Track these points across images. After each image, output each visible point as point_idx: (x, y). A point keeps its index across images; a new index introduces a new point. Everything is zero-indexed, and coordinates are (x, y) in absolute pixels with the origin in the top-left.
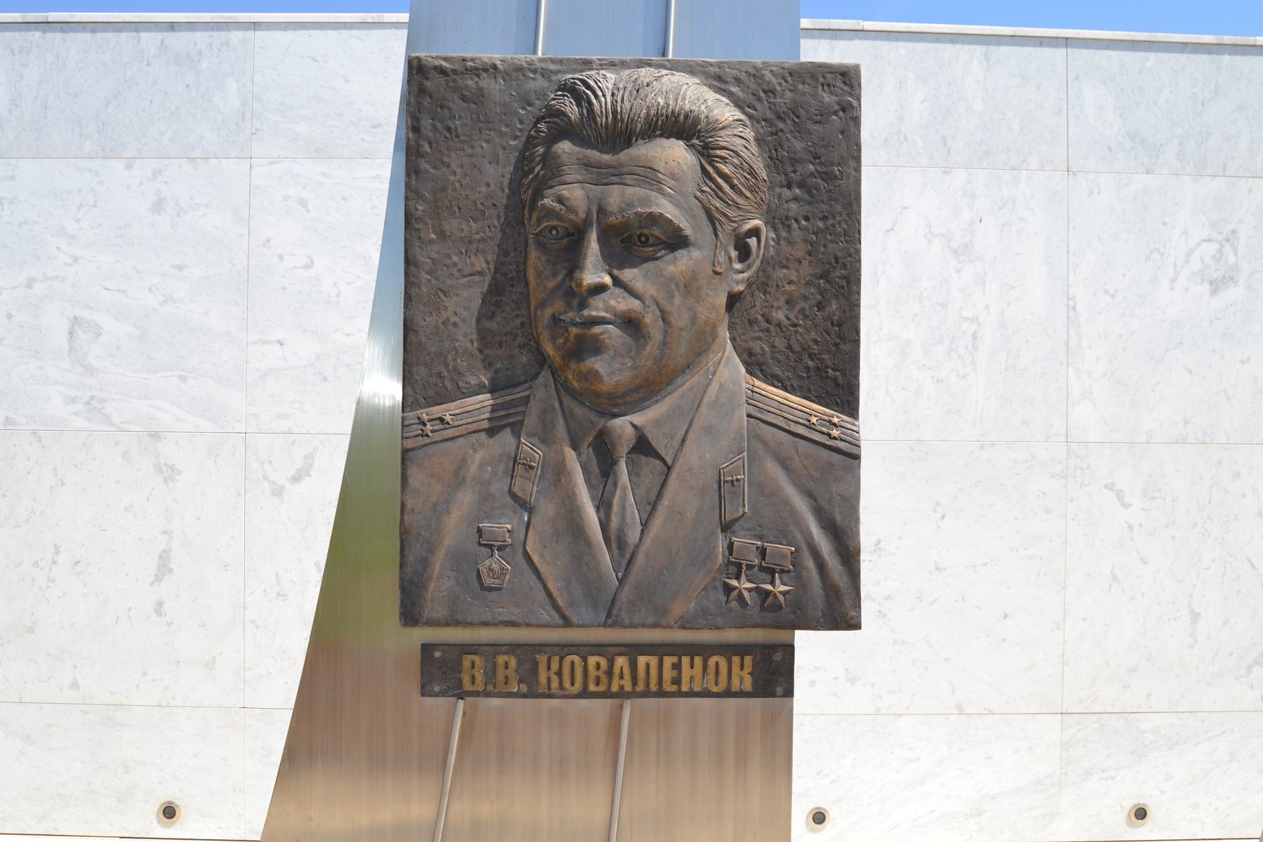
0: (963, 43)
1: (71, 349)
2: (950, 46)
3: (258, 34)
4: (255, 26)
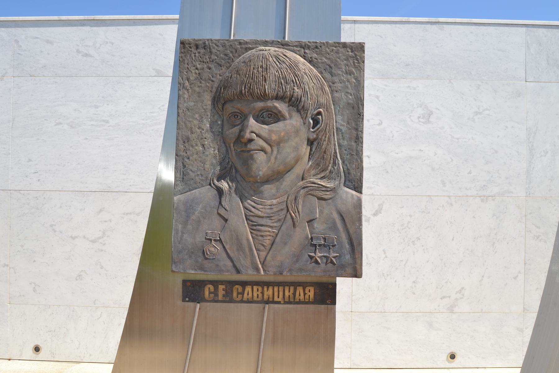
3: (357, 25)
4: (355, 22)
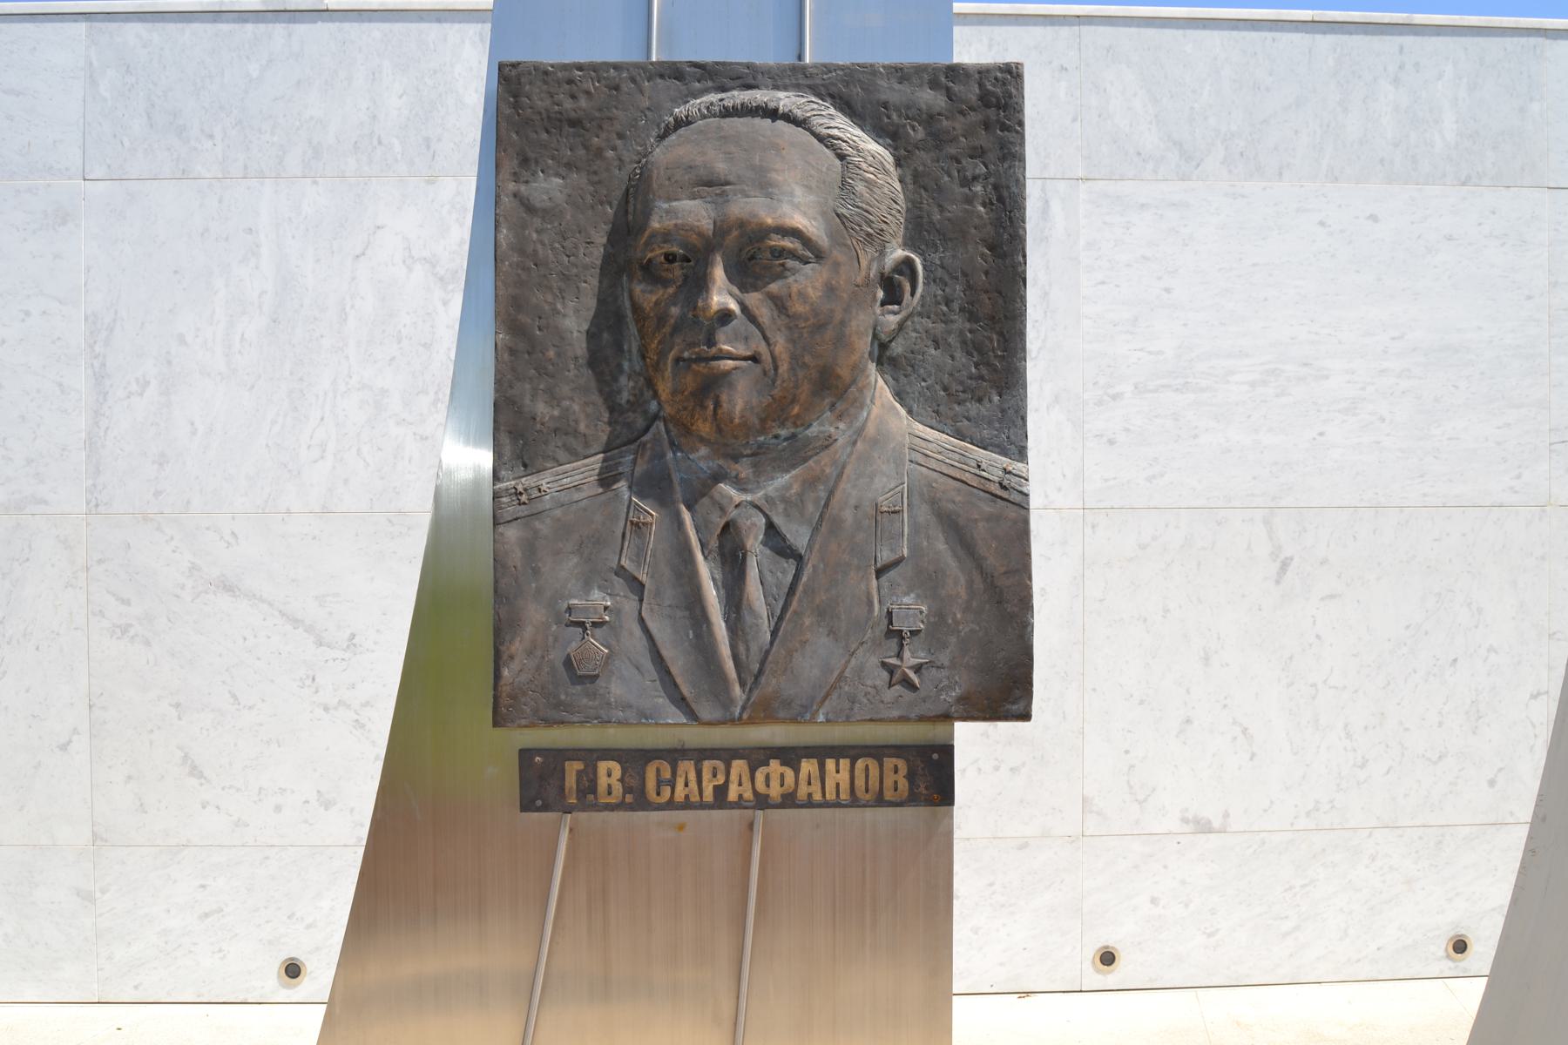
0: (453, 21)
2: (435, 26)
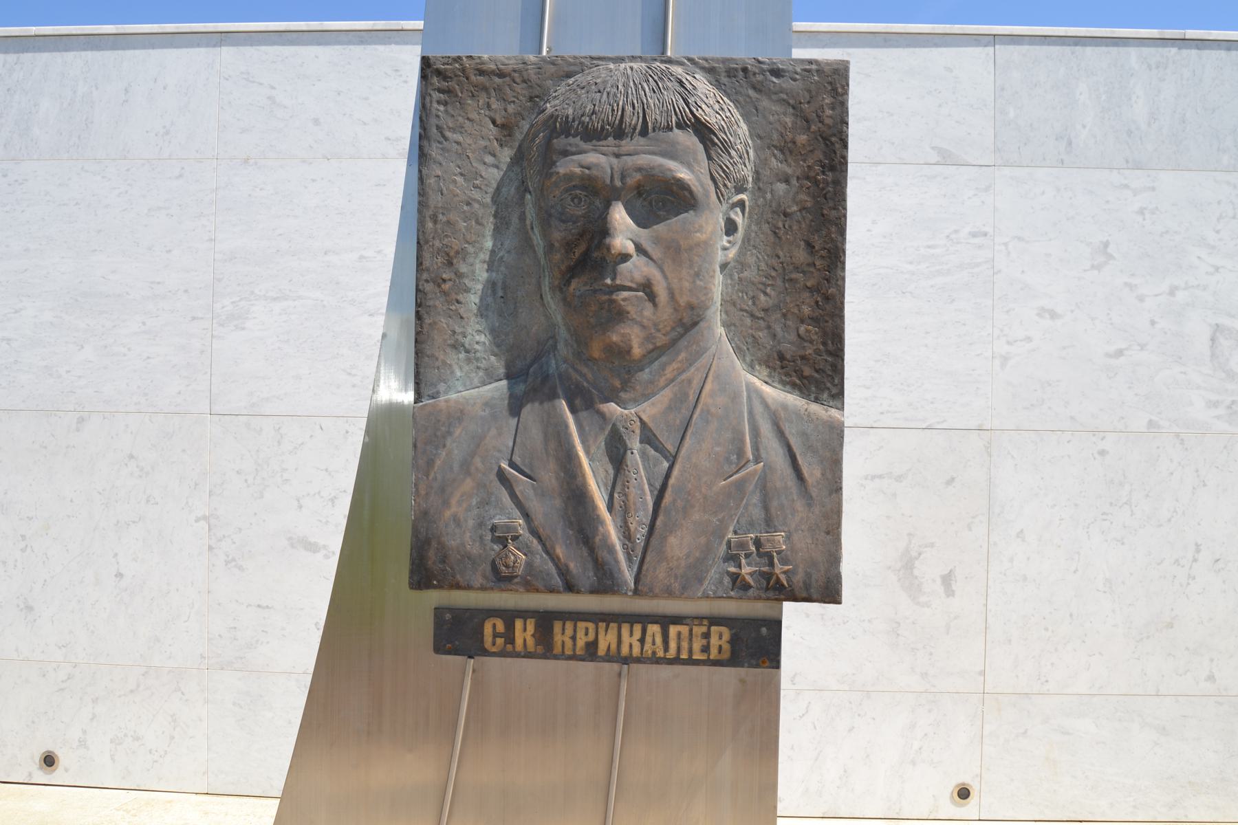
1: (1213, 355)
